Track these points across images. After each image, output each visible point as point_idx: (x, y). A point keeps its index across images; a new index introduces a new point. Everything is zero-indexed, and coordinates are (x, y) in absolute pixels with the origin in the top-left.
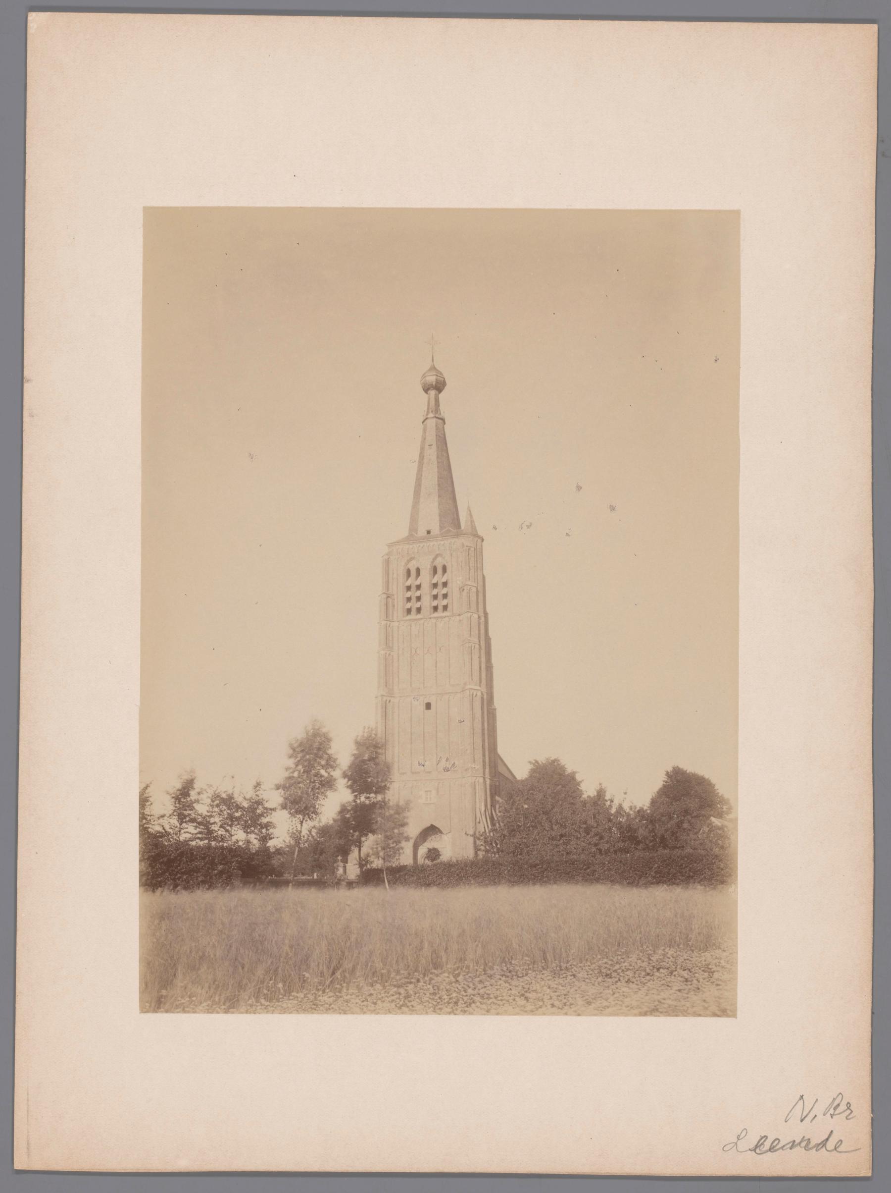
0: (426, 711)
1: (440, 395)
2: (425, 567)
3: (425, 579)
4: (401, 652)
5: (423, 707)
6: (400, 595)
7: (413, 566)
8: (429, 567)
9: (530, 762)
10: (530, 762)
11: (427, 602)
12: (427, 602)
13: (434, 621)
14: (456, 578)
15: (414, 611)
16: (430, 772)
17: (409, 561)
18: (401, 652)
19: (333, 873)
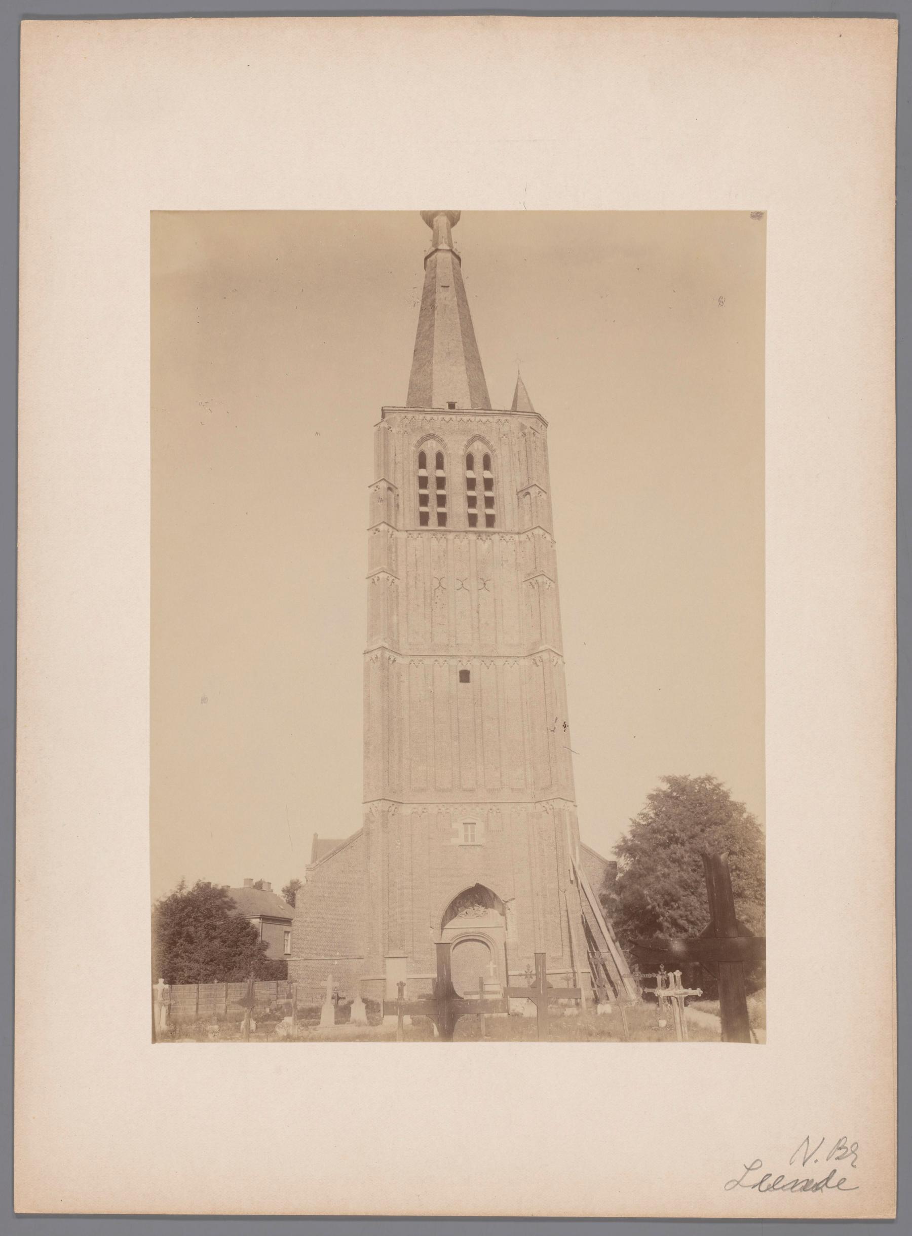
8: (461, 453)
17: (423, 440)
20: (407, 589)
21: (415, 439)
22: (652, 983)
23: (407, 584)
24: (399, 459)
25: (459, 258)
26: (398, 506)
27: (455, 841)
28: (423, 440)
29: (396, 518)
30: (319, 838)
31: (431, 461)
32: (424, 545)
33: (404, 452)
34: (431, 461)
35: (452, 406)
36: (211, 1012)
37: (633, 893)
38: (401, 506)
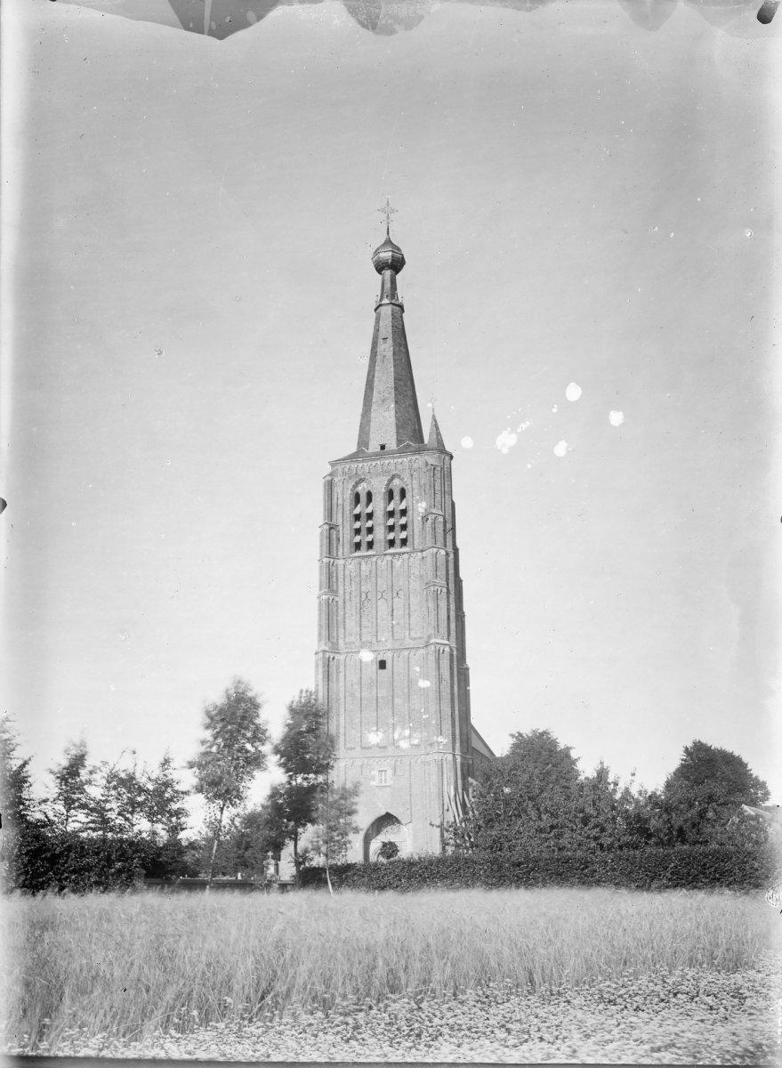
0: (381, 671)
2: (378, 486)
6: (345, 533)
8: (384, 490)
9: (512, 736)
10: (512, 736)
11: (380, 534)
12: (380, 534)
17: (357, 484)
18: (347, 598)
20: (345, 603)
21: (385, 480)
22: (746, 963)
23: (344, 600)
24: (340, 502)
25: (401, 307)
26: (339, 539)
27: (372, 783)
28: (390, 481)
29: (337, 547)
30: (28, 767)
31: (363, 498)
32: (349, 565)
33: (344, 494)
34: (363, 498)
35: (383, 447)
36: (156, 825)
37: (71, 917)
38: (341, 539)
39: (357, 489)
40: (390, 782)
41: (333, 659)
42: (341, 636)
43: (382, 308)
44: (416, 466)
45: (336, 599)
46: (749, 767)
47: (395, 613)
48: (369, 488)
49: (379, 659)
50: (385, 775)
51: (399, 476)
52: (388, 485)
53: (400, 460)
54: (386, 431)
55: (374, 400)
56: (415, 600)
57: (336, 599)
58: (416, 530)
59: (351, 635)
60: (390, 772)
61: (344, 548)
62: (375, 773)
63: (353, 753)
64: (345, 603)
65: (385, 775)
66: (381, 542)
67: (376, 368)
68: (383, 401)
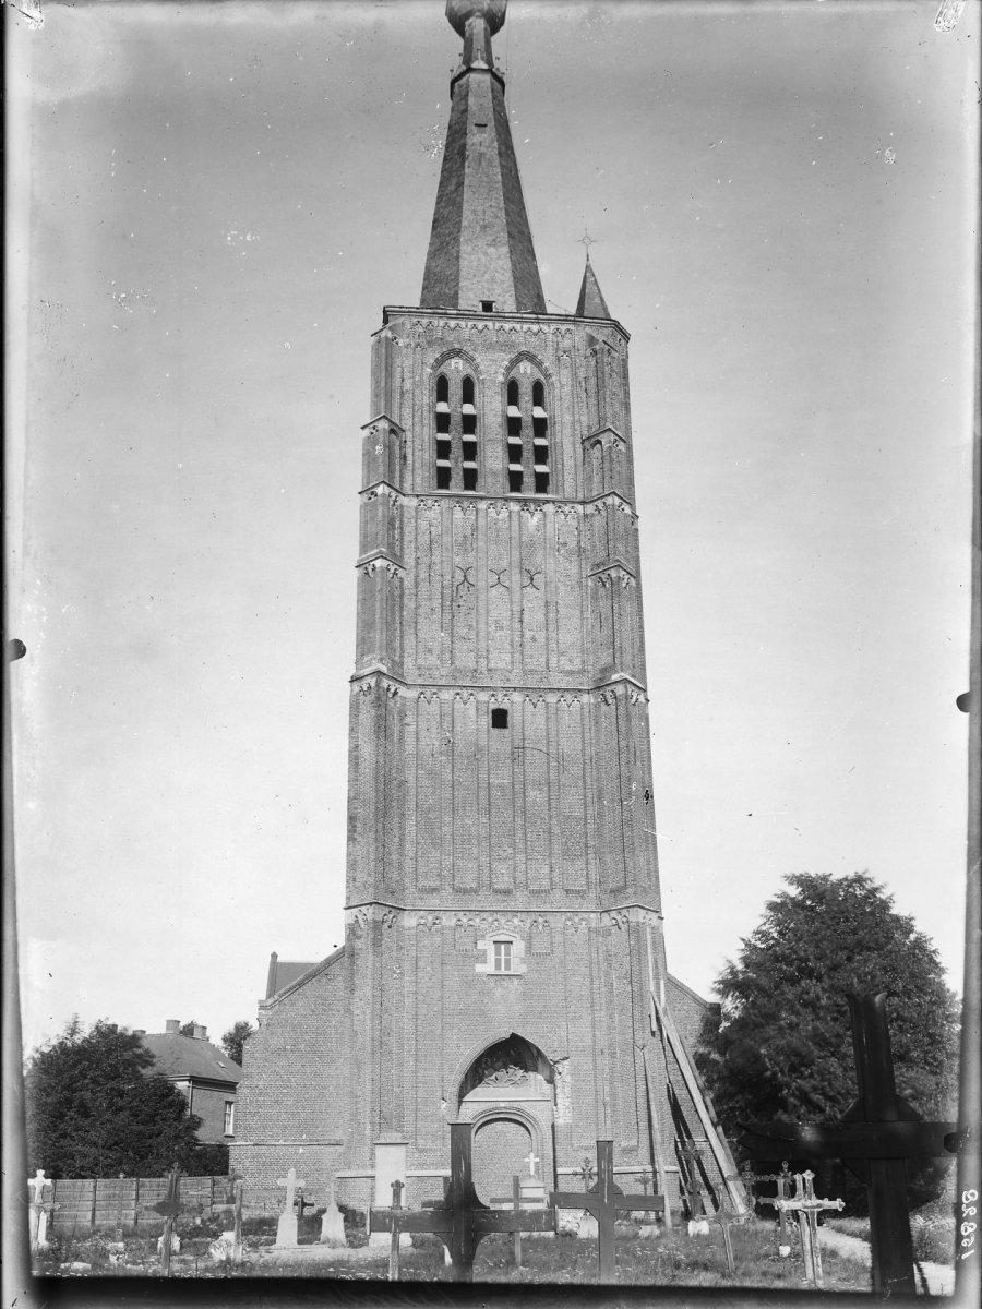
0: (495, 732)
1: (494, 39)
2: (492, 371)
3: (491, 407)
4: (423, 575)
5: (486, 720)
6: (420, 438)
7: (456, 368)
8: (501, 378)
9: (931, 939)
10: (931, 939)
11: (493, 460)
12: (493, 460)
13: (515, 507)
14: (568, 416)
15: (457, 479)
16: (507, 892)
17: (445, 358)
18: (423, 575)
19: (706, 1238)
20: (417, 585)
21: (505, 359)
23: (417, 576)
24: (408, 385)
25: (502, 84)
27: (479, 968)
31: (455, 390)
33: (416, 372)
34: (455, 390)
35: (487, 306)
39: (443, 369)
40: (518, 967)
41: (395, 693)
42: (409, 650)
43: (473, 77)
44: (566, 343)
45: (401, 573)
46: (920, 927)
47: (526, 618)
48: (470, 371)
49: (493, 706)
50: (508, 953)
51: (530, 357)
52: (509, 369)
53: (535, 328)
54: (493, 280)
55: (465, 223)
56: (566, 597)
57: (401, 573)
58: (569, 463)
59: (430, 651)
60: (519, 947)
61: (419, 475)
62: (487, 945)
63: (433, 902)
64: (417, 585)
65: (508, 953)
66: (495, 474)
67: (467, 171)
68: (484, 227)
